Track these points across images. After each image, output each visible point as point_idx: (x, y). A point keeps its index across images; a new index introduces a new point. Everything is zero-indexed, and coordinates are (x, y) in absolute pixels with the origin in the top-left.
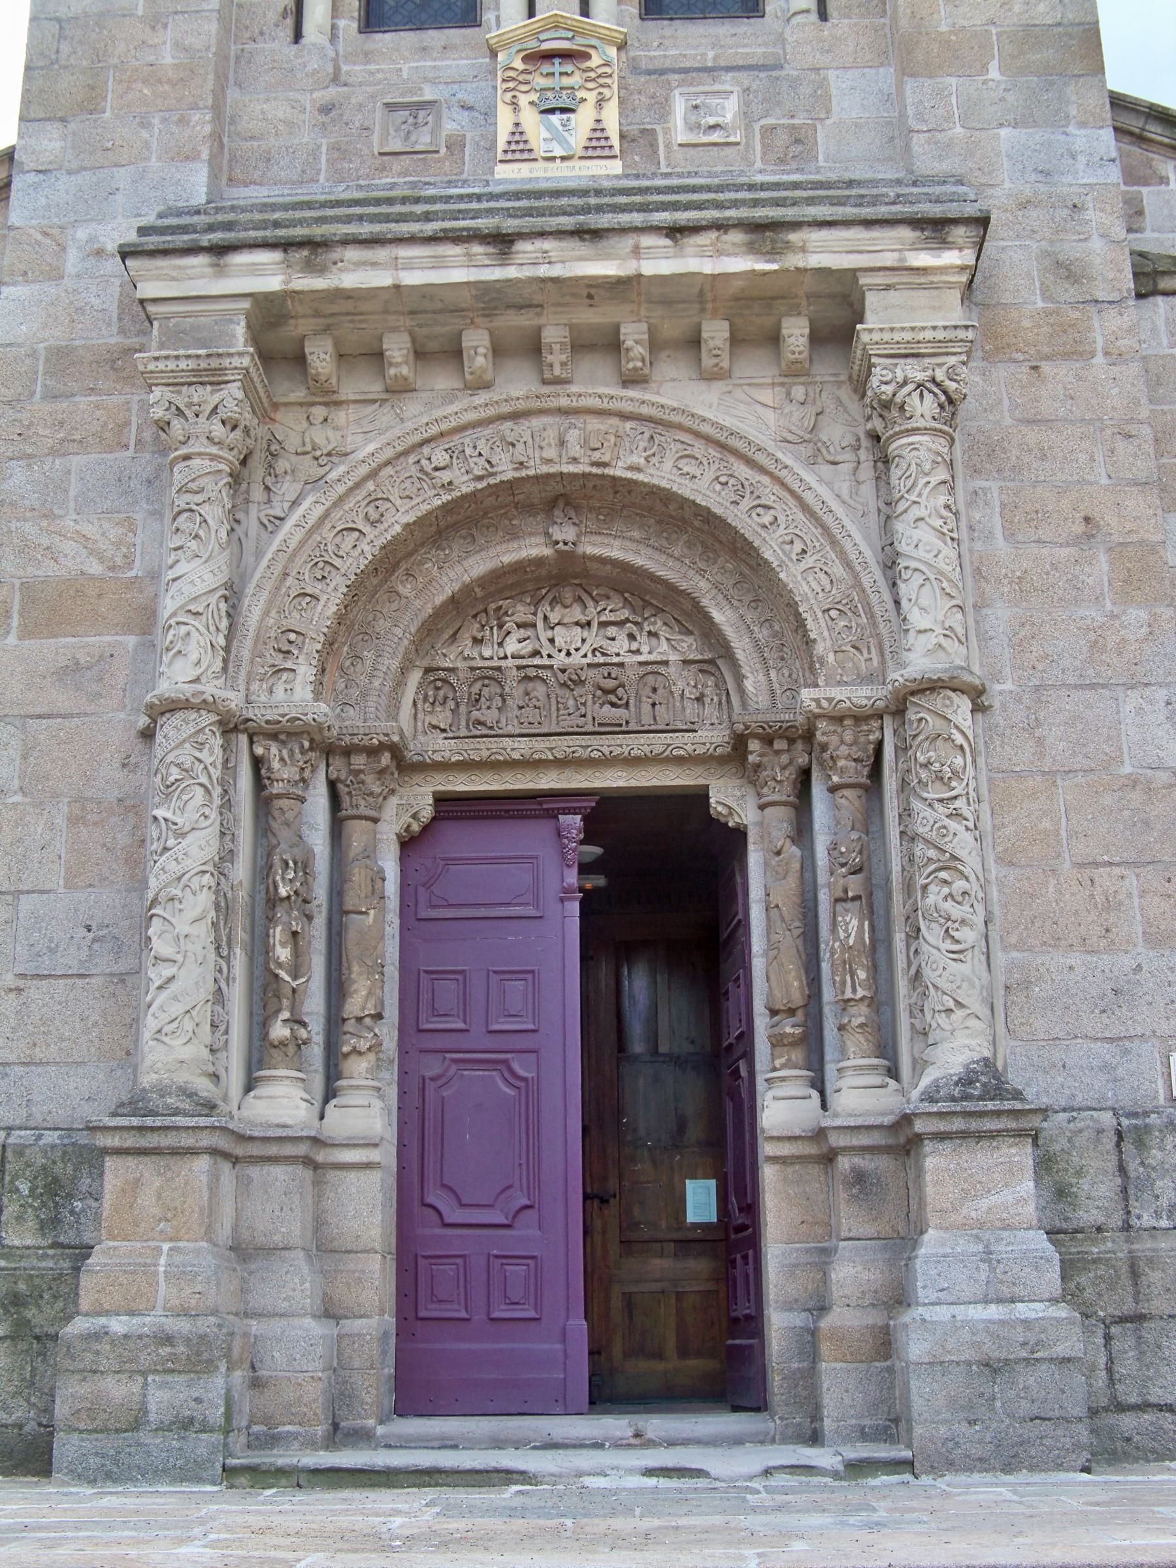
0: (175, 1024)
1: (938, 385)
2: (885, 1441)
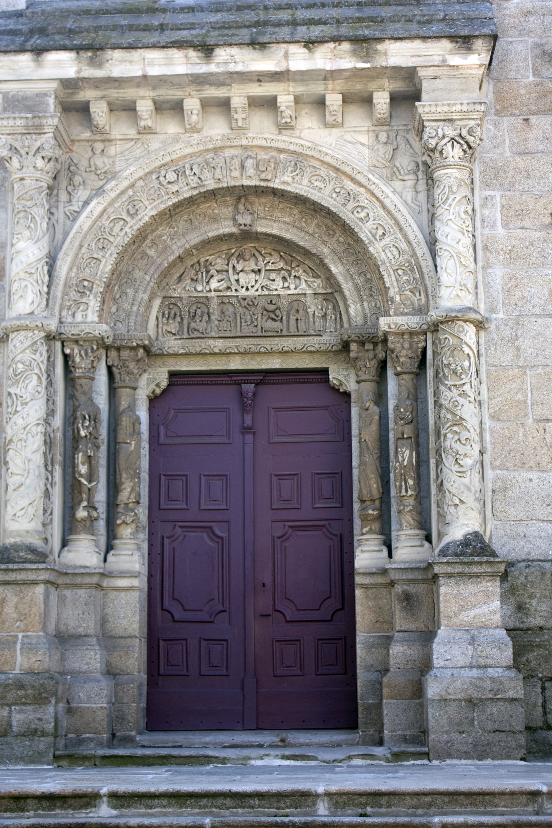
0: (23, 511)
1: (463, 138)
2: (418, 744)
